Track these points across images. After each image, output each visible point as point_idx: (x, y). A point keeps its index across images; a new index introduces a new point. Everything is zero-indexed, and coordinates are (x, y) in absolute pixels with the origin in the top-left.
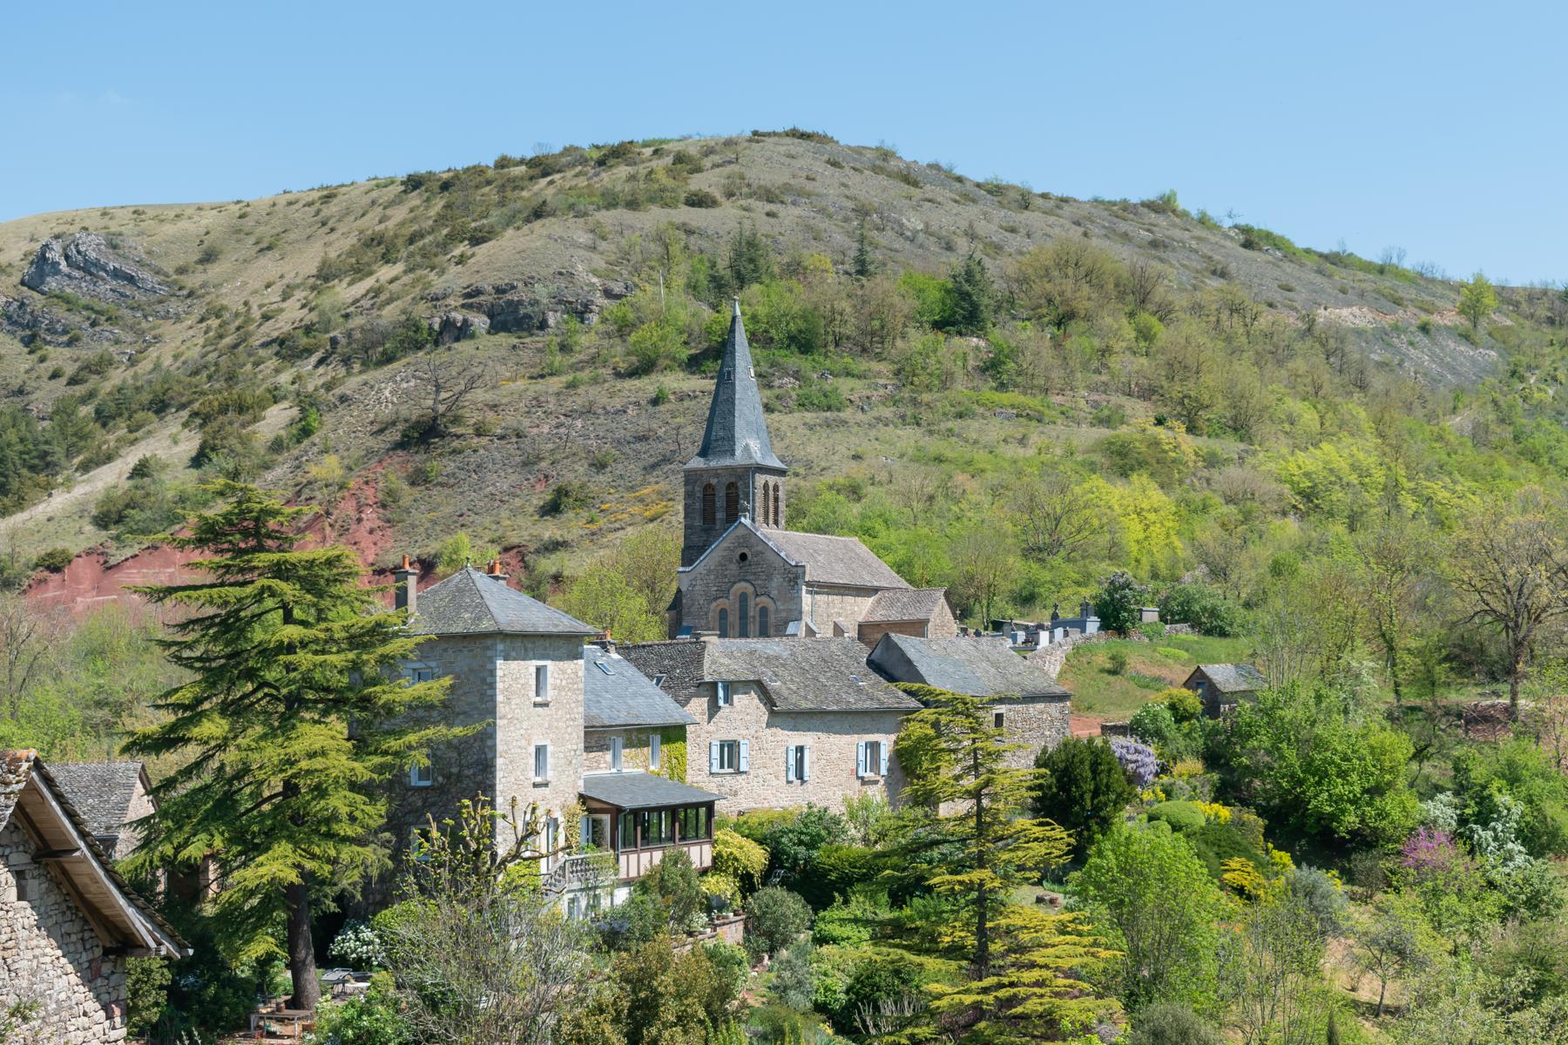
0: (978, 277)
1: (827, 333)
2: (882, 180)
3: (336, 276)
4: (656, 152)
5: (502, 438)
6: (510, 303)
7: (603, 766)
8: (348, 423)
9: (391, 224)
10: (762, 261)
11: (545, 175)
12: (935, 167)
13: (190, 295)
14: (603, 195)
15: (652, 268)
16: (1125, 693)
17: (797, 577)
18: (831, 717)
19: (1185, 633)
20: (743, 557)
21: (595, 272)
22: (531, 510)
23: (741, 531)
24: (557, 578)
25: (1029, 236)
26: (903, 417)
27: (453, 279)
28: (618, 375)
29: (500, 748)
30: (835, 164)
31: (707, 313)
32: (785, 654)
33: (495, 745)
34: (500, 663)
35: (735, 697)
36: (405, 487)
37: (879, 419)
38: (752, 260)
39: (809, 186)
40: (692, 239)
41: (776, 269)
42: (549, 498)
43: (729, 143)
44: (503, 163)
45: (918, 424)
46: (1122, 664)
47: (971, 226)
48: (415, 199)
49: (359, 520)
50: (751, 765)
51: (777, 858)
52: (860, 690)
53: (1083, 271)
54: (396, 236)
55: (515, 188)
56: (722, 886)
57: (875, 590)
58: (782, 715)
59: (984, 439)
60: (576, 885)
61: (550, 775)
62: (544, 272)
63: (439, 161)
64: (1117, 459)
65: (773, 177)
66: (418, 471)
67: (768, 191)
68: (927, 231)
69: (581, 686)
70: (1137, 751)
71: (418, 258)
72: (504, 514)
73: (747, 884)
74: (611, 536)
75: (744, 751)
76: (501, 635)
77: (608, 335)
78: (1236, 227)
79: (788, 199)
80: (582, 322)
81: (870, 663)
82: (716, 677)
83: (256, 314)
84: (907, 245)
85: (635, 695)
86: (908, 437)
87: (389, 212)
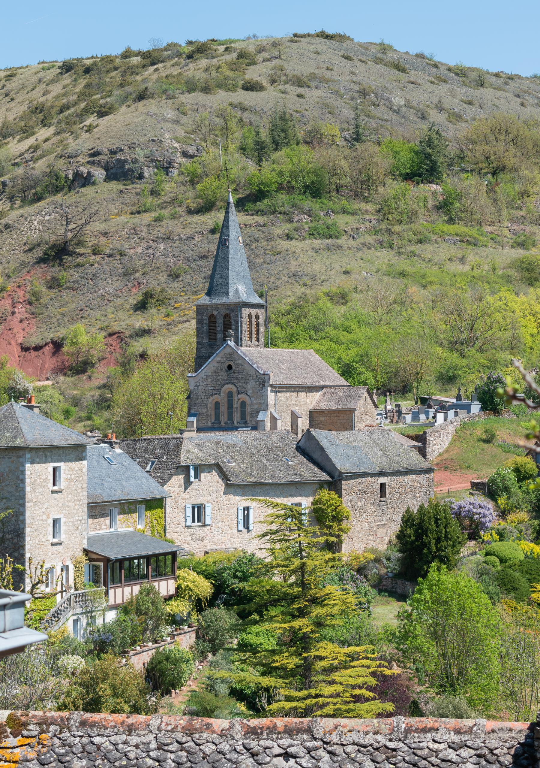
0: (436, 142)
1: (330, 184)
2: (381, 68)
3: (10, 135)
4: (227, 49)
5: (110, 256)
6: (119, 161)
7: (103, 527)
8: (10, 244)
9: (50, 97)
10: (290, 131)
11: (153, 64)
12: (421, 56)
14: (186, 83)
15: (216, 136)
16: (494, 456)
17: (264, 382)
20: (230, 367)
21: (177, 140)
22: (128, 307)
23: (228, 350)
24: (143, 356)
25: (481, 107)
26: (381, 243)
27: (81, 143)
28: (190, 212)
29: (28, 521)
30: (348, 58)
31: (252, 167)
32: (241, 443)
33: (25, 520)
34: (28, 466)
35: (202, 475)
36: (45, 289)
37: (364, 244)
38: (283, 131)
39: (328, 75)
40: (246, 114)
41: (300, 136)
42: (140, 298)
43: (275, 44)
44: (127, 55)
45: (391, 248)
46: (493, 436)
47: (440, 102)
48: (67, 79)
49: (13, 313)
50: (213, 520)
51: (219, 588)
52: (289, 468)
53: (511, 136)
54: (52, 107)
55: (132, 74)
56: (180, 607)
57: (322, 387)
58: (233, 487)
59: (436, 259)
60: (79, 610)
61: (63, 537)
62: (142, 140)
63: (85, 50)
64: (526, 274)
65: (305, 69)
66: (54, 279)
67: (299, 79)
68: (408, 105)
69: (85, 478)
70: (480, 507)
71: (63, 125)
72: (110, 310)
73: (199, 606)
74: (180, 326)
75: (208, 511)
76: (26, 448)
77: (183, 183)
79: (313, 84)
80: (167, 174)
81: (298, 448)
82: (189, 462)
84: (394, 116)
85: (128, 479)
86: (383, 257)
87: (50, 88)
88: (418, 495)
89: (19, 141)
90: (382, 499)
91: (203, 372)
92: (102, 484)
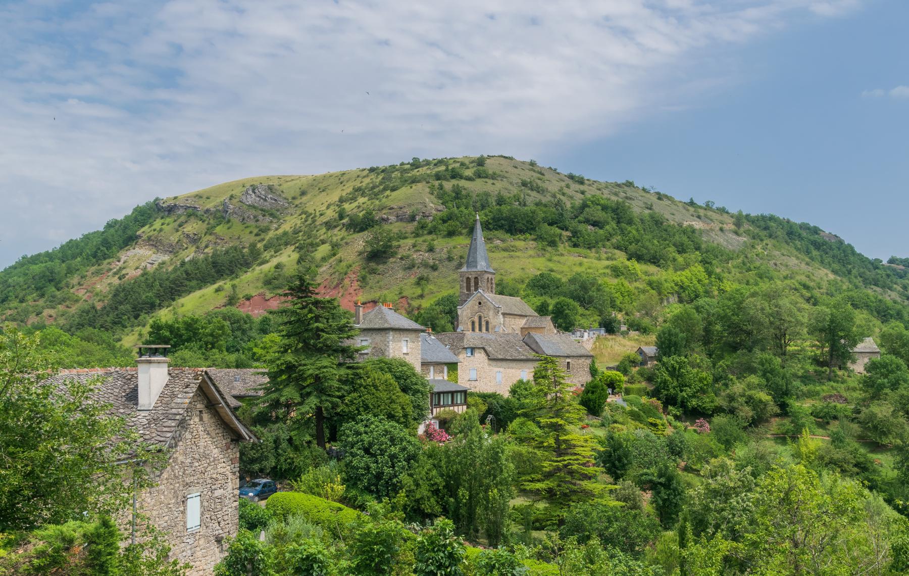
19: (633, 334)
39: (506, 175)
44: (402, 164)
52: (519, 352)
83: (318, 214)
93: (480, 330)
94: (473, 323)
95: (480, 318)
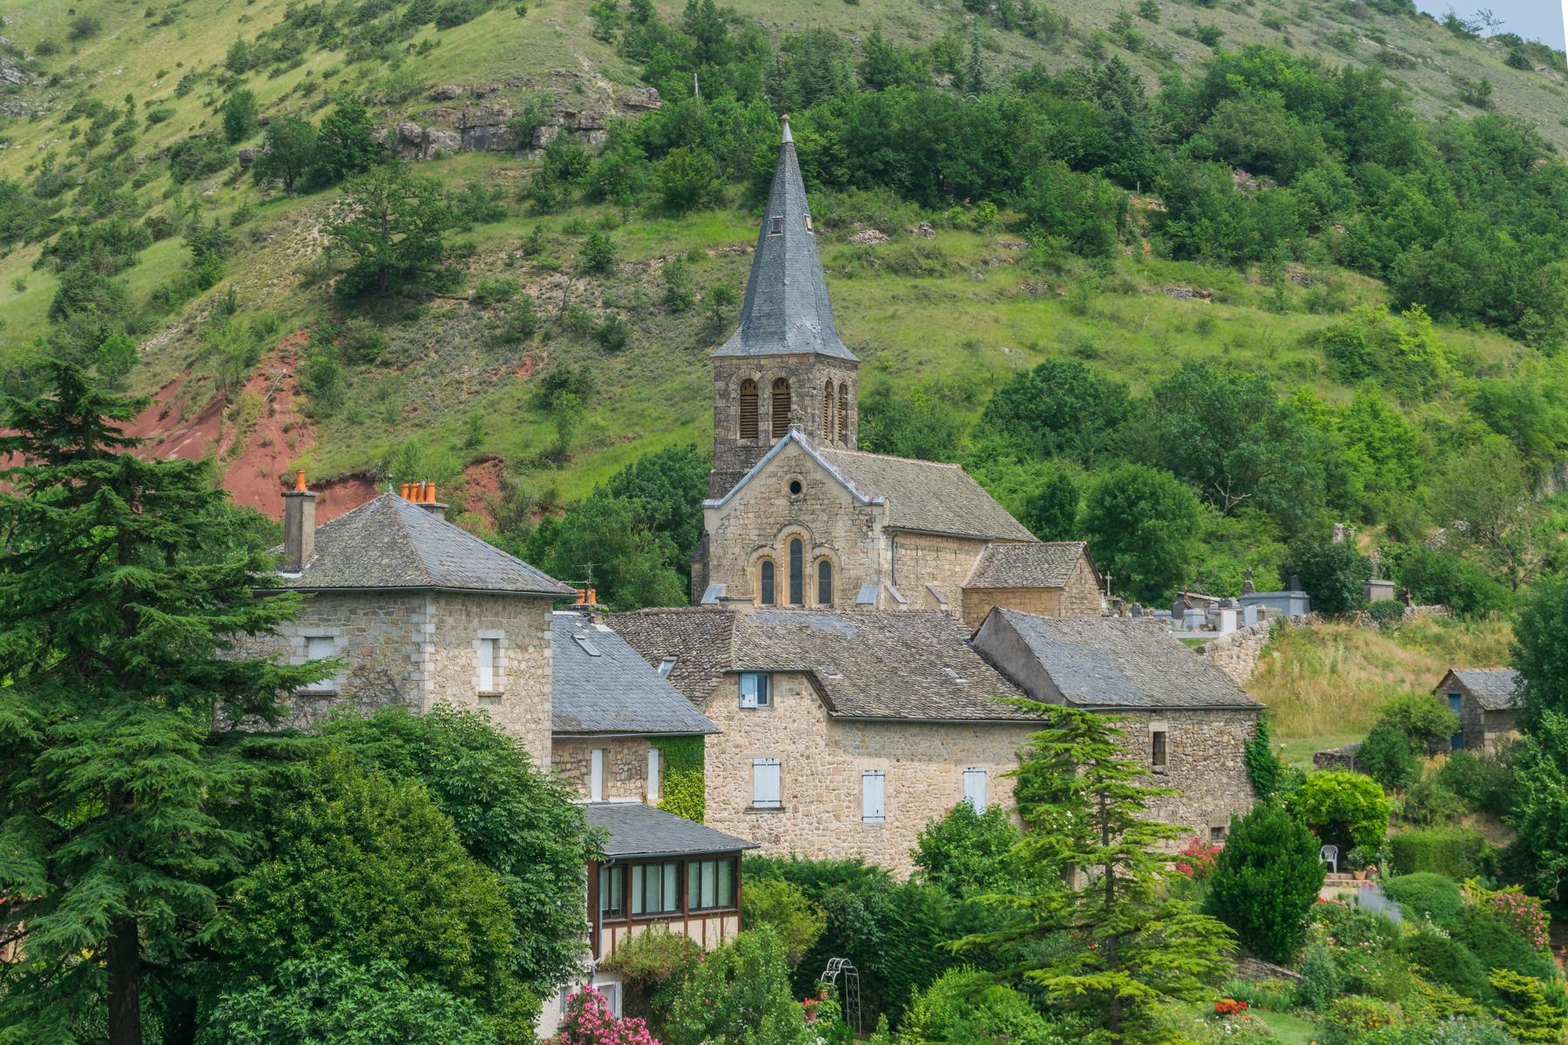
13: (55, 82)
18: (915, 730)
69: (548, 671)
78: (1499, 37)
83: (141, 116)
85: (628, 688)
88: (1230, 764)
89: (271, 78)
90: (1158, 768)
91: (738, 496)
92: (575, 695)
93: (797, 597)
94: (768, 568)
95: (796, 547)
